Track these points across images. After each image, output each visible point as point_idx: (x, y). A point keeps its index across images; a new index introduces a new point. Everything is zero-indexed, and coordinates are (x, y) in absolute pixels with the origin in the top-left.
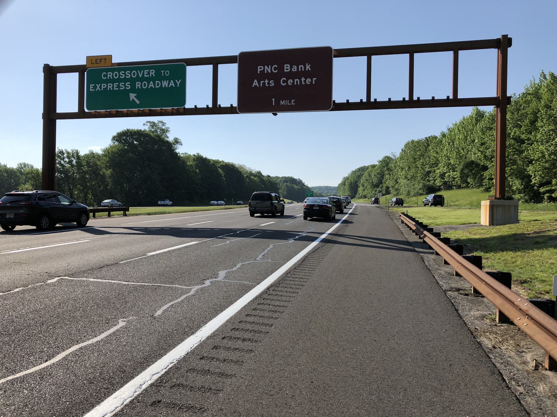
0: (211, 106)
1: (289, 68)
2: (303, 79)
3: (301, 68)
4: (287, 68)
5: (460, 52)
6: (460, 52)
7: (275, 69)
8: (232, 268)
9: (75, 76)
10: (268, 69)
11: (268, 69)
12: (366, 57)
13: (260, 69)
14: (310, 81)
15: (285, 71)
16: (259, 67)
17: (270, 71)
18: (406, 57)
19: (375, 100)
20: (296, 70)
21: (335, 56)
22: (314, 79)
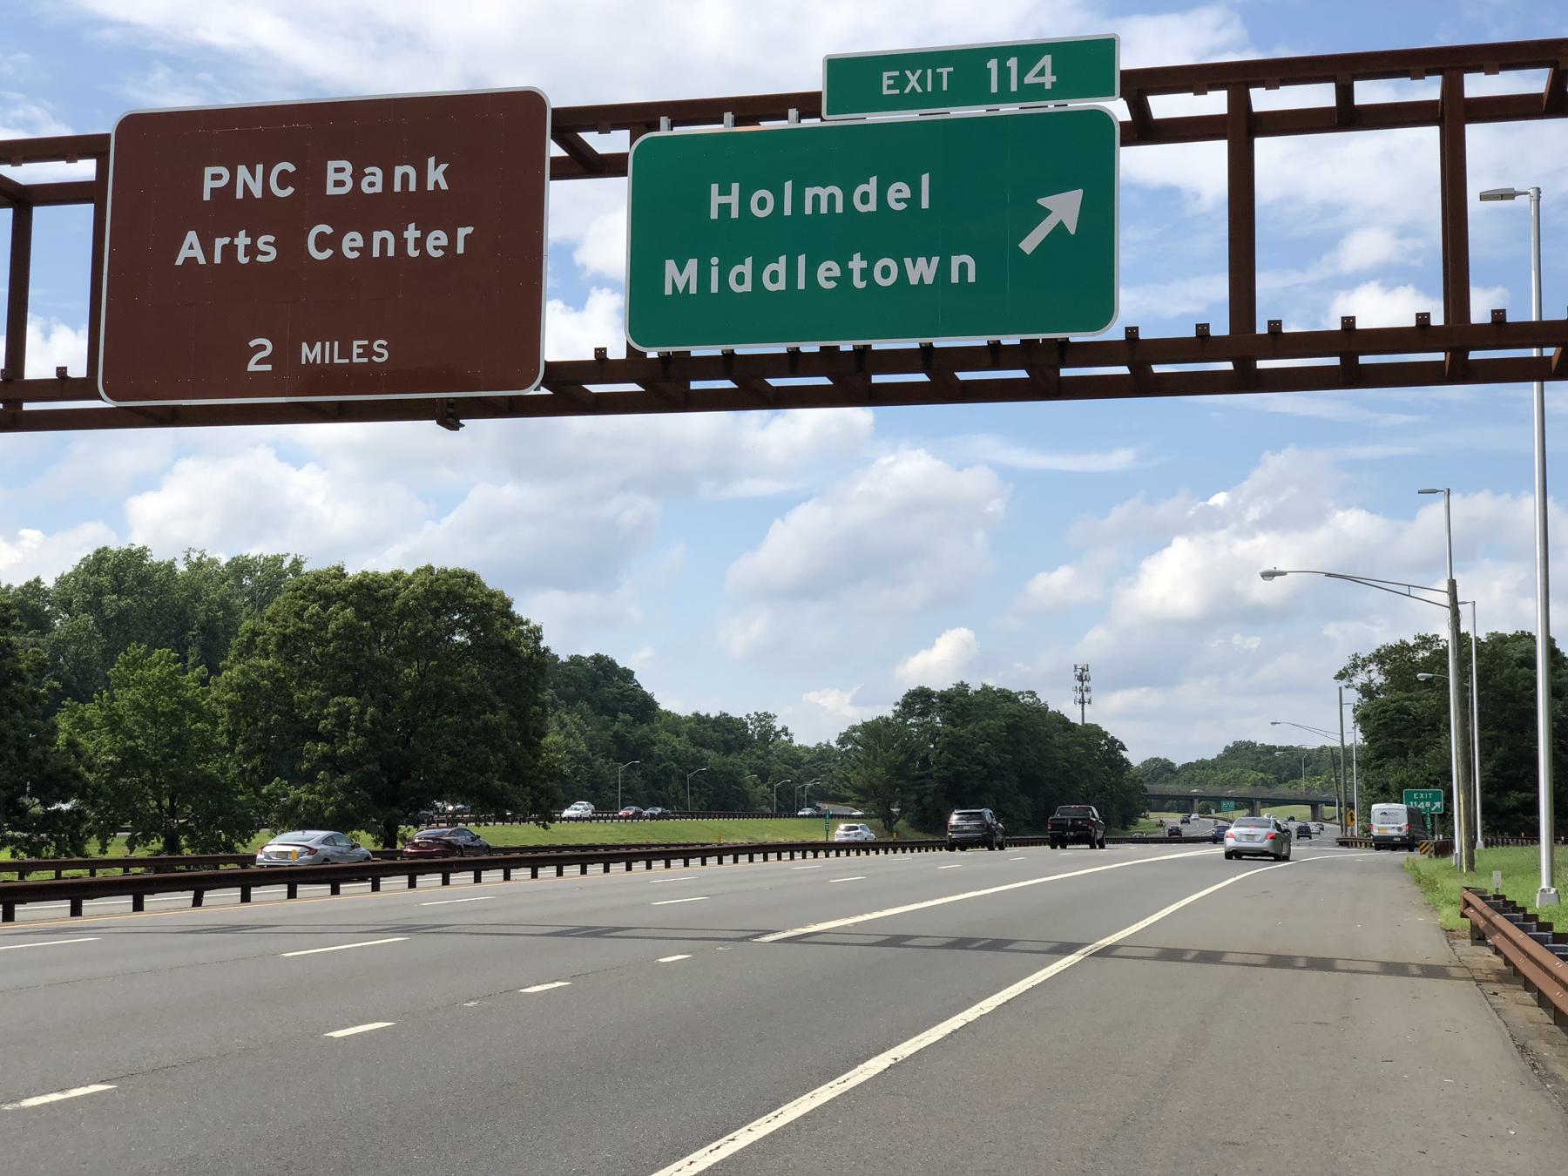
1: (346, 177)
2: (411, 233)
3: (405, 177)
4: (338, 176)
7: (284, 179)
10: (249, 180)
11: (249, 180)
13: (213, 178)
15: (331, 190)
16: (209, 171)
20: (378, 189)
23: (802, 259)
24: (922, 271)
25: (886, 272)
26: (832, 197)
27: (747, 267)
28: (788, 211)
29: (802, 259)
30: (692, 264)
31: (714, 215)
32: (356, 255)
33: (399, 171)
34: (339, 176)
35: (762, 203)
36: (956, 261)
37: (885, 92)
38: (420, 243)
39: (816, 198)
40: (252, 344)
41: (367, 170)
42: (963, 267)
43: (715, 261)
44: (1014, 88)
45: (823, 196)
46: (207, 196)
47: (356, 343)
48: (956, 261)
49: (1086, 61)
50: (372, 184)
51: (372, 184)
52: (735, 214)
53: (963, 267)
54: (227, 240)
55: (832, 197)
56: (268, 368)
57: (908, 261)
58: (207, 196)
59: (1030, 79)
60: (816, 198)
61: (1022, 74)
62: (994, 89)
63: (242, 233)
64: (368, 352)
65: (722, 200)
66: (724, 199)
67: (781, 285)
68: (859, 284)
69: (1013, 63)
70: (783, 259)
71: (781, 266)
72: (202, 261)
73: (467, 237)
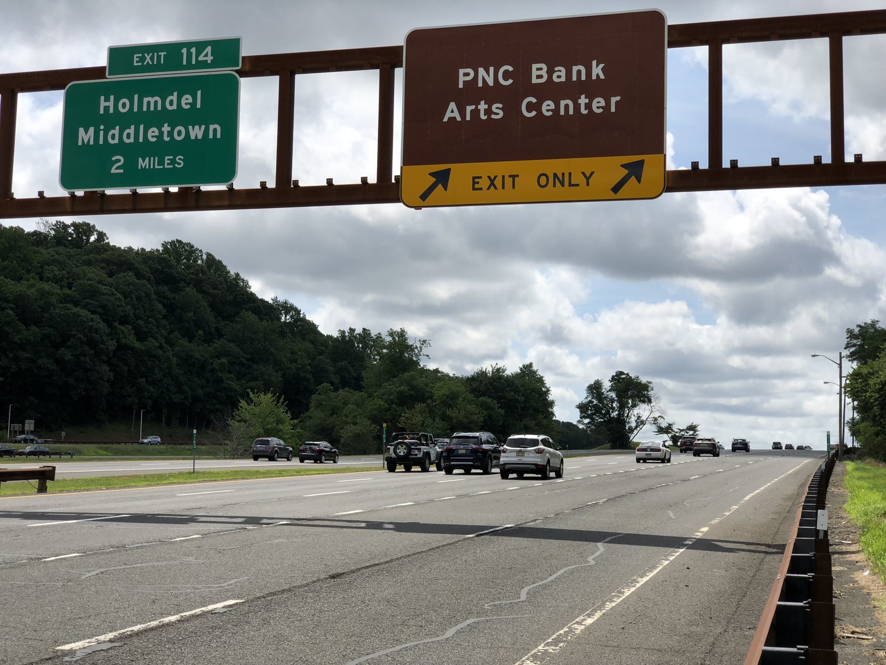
0: (373, 179)
1: (544, 73)
2: (583, 100)
3: (579, 72)
4: (538, 72)
5: (845, 39)
6: (846, 40)
7: (506, 75)
8: (443, 631)
9: (364, 86)
10: (486, 76)
11: (486, 76)
12: (276, 78)
13: (464, 75)
14: (552, 106)
15: (535, 81)
16: (462, 71)
17: (491, 82)
18: (821, 45)
19: (858, 157)
20: (563, 79)
21: (672, 44)
22: (614, 100)
23: (142, 127)
24: (196, 132)
25: (179, 133)
26: (156, 102)
27: (116, 131)
28: (136, 110)
29: (142, 127)
30: (92, 130)
31: (102, 112)
32: (550, 113)
33: (575, 69)
34: (539, 73)
35: (124, 105)
36: (212, 127)
37: (135, 64)
38: (588, 106)
39: (149, 103)
40: (114, 159)
41: (556, 69)
42: (215, 130)
43: (102, 127)
44: (194, 63)
45: (152, 101)
46: (461, 86)
47: (166, 158)
48: (212, 127)
49: (226, 49)
50: (559, 77)
51: (559, 77)
52: (111, 111)
53: (215, 130)
54: (473, 107)
55: (156, 102)
56: (122, 171)
57: (190, 127)
58: (461, 86)
59: (201, 58)
60: (149, 103)
61: (197, 56)
62: (185, 63)
63: (482, 102)
64: (173, 162)
65: (105, 104)
66: (107, 104)
67: (132, 140)
68: (166, 139)
69: (193, 50)
70: (133, 127)
71: (131, 130)
72: (459, 119)
73: (617, 102)
